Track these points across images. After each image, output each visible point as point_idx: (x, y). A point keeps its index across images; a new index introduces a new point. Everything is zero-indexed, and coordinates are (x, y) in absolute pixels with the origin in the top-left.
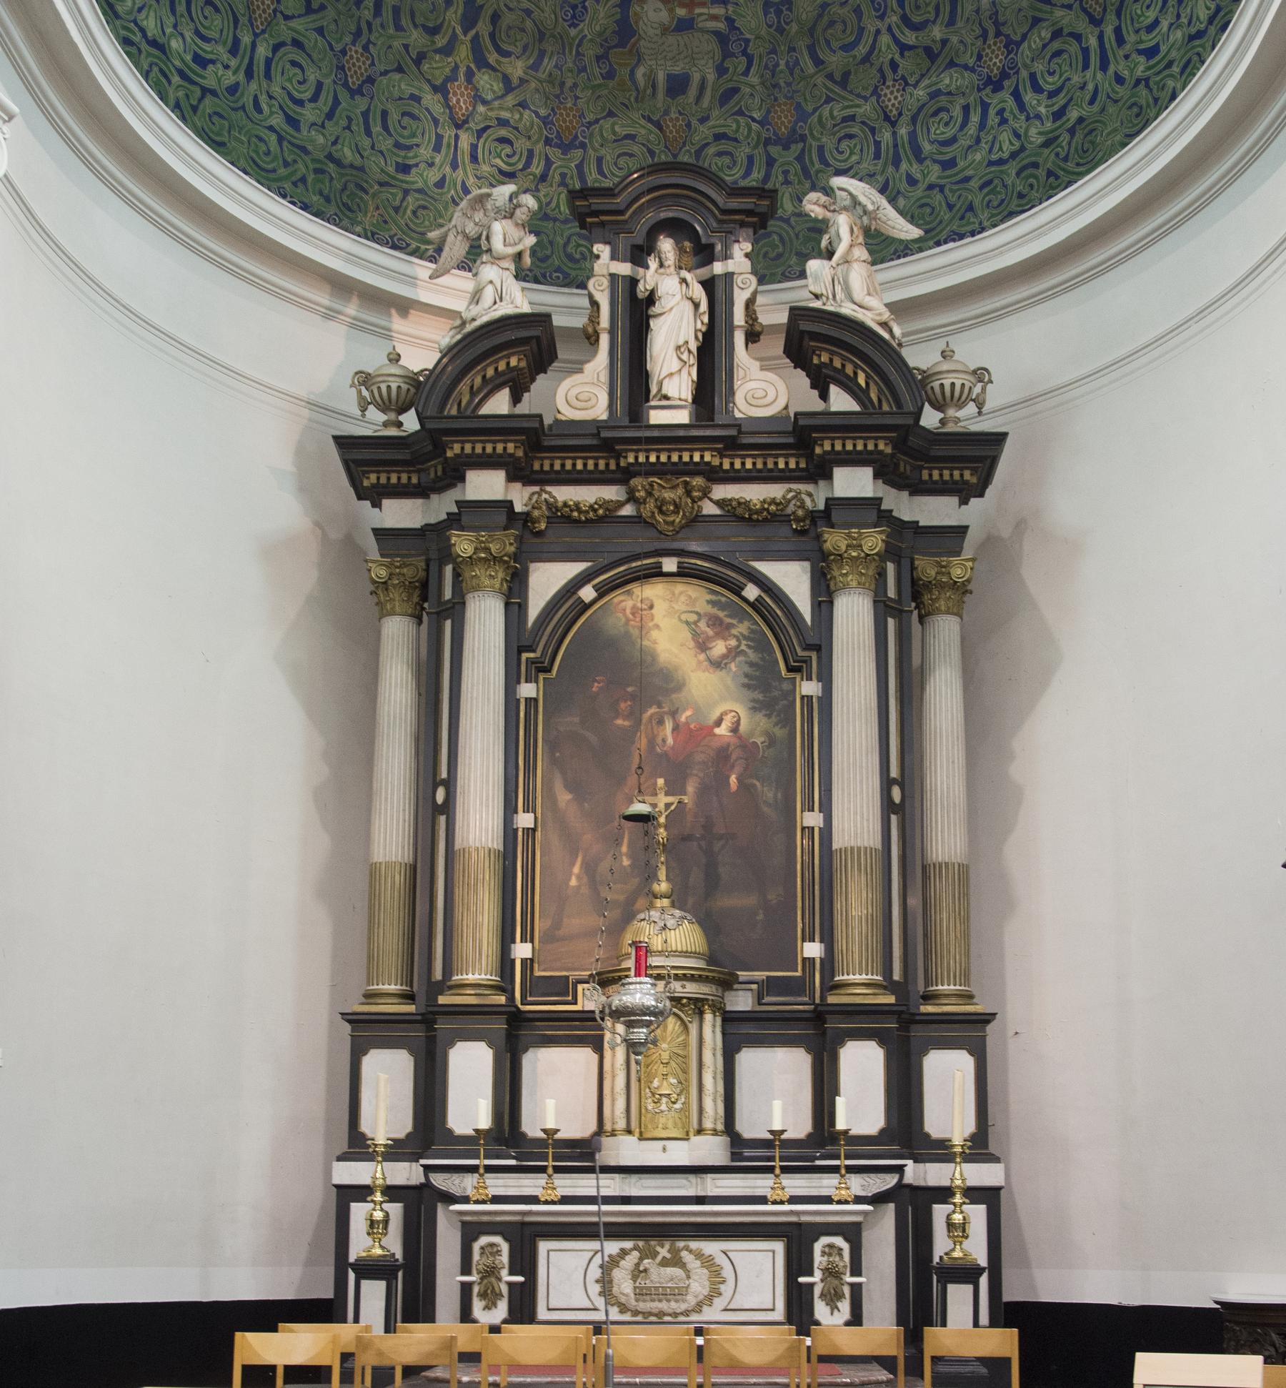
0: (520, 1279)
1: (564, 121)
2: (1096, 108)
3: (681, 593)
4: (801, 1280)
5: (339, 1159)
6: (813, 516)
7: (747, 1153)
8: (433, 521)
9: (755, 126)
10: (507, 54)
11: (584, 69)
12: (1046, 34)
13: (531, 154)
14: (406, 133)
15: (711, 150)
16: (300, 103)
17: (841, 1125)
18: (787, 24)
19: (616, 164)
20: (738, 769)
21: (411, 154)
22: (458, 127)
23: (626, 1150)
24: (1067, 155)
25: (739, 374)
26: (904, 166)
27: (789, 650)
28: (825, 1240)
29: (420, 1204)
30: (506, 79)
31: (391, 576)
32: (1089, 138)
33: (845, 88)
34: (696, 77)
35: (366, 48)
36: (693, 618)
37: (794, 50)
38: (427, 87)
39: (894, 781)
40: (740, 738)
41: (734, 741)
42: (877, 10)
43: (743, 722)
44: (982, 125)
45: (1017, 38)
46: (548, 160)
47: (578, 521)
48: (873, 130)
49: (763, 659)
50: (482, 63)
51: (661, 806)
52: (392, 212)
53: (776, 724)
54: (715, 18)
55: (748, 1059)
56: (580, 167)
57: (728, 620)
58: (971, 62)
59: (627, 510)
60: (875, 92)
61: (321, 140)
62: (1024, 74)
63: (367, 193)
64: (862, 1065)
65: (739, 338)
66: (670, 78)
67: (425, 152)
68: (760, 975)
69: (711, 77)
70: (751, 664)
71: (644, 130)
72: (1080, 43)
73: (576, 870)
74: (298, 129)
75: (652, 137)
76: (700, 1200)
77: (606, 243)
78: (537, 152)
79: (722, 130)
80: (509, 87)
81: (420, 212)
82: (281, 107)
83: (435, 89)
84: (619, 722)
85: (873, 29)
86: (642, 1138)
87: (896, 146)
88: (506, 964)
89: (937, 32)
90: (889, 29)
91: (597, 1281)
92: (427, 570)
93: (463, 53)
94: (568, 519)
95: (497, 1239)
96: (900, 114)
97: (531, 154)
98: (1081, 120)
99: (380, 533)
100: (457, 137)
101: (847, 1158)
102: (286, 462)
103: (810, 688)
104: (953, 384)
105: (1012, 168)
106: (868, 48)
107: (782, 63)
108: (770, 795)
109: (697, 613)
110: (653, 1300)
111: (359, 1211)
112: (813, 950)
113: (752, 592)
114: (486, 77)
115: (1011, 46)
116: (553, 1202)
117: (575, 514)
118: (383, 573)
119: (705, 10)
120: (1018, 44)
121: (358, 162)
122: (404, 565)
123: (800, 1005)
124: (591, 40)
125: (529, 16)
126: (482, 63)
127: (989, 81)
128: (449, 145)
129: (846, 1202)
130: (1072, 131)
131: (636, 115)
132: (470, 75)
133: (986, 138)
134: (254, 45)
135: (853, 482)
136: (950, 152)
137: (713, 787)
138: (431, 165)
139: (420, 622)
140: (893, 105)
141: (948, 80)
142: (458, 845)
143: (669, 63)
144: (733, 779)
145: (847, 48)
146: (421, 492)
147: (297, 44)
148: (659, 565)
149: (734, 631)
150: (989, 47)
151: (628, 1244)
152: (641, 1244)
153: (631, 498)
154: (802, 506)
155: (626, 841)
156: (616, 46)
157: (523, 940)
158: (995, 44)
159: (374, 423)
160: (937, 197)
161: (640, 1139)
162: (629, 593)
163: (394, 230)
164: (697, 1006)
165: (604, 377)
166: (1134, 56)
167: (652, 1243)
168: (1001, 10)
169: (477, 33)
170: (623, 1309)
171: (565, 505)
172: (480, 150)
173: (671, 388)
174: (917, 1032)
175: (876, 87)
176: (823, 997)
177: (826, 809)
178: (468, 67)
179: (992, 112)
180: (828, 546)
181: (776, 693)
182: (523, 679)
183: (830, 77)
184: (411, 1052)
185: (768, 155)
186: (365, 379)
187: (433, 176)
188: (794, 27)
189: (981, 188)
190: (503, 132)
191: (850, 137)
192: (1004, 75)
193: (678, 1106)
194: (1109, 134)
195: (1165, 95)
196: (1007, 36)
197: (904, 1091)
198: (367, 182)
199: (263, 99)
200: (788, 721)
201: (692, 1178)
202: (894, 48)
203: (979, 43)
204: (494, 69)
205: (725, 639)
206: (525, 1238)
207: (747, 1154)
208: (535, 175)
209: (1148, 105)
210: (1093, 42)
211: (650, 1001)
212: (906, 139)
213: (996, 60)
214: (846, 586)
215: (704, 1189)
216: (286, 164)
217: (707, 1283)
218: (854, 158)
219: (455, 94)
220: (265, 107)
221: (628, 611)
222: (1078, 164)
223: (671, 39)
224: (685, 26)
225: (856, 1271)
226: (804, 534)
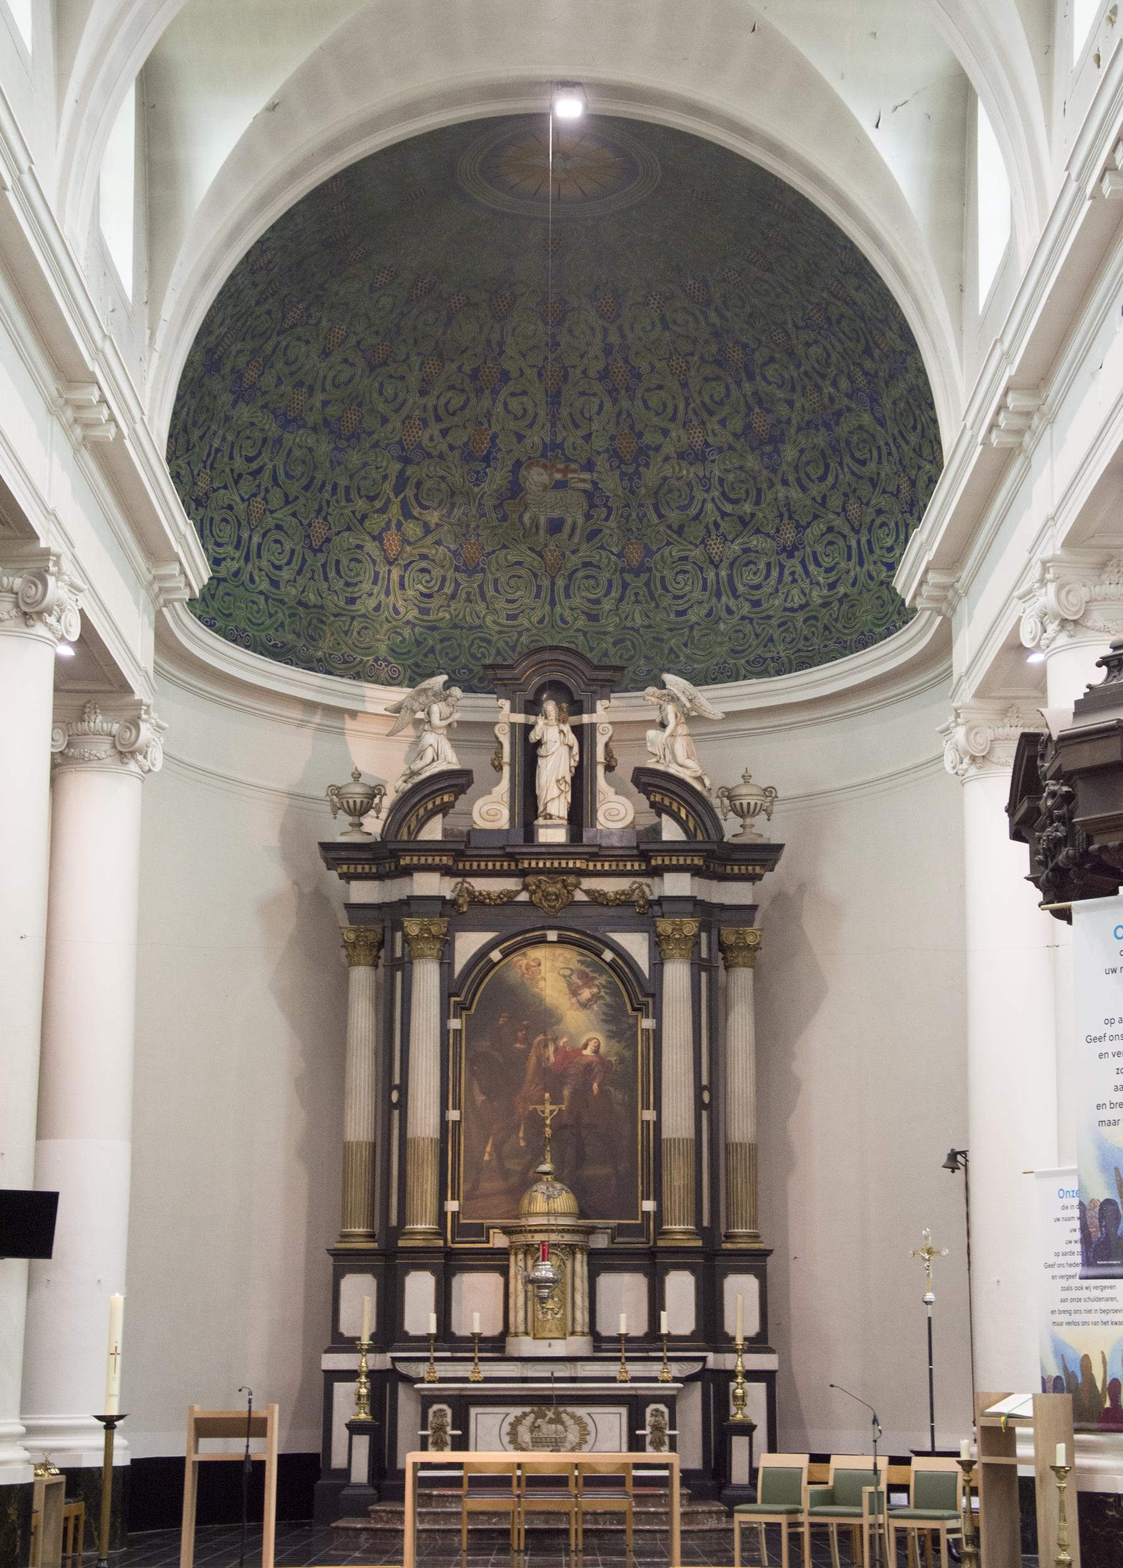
0: (459, 1432)
1: (469, 553)
2: (855, 590)
4: (638, 1432)
5: (326, 1352)
6: (651, 903)
7: (604, 1346)
8: (387, 900)
9: (613, 558)
11: (484, 515)
13: (444, 579)
14: (353, 574)
15: (580, 574)
16: (279, 568)
17: (664, 1330)
20: (598, 1079)
22: (390, 564)
23: (526, 1346)
25: (600, 797)
26: (724, 599)
27: (631, 996)
28: (653, 1406)
29: (383, 1386)
30: (426, 525)
33: (680, 536)
34: (569, 521)
35: (325, 519)
36: (568, 972)
37: (642, 505)
38: (367, 538)
39: (705, 1088)
40: (600, 1057)
41: (596, 1059)
44: (780, 581)
45: (804, 524)
46: (456, 582)
48: (701, 569)
50: (407, 514)
51: (547, 1111)
52: (343, 635)
54: (583, 481)
55: (605, 1281)
56: (481, 587)
57: (592, 974)
58: (772, 532)
59: (523, 897)
60: (703, 542)
61: (294, 592)
62: (808, 550)
64: (681, 1287)
65: (600, 770)
66: (551, 521)
67: (366, 586)
68: (613, 1222)
69: (580, 521)
70: (607, 1005)
71: (529, 558)
73: (488, 1149)
74: (278, 588)
75: (535, 564)
76: (573, 1380)
77: (507, 698)
78: (448, 577)
79: (588, 560)
80: (427, 529)
82: (267, 575)
83: (374, 538)
84: (518, 1045)
85: (701, 499)
86: (535, 1338)
87: (718, 583)
88: (442, 1214)
89: (748, 508)
90: (713, 500)
92: (383, 935)
93: (395, 510)
94: (483, 903)
95: (444, 1407)
96: (721, 561)
97: (444, 579)
98: (846, 595)
99: (349, 907)
100: (390, 571)
102: (272, 838)
103: (647, 1023)
104: (749, 804)
105: (800, 617)
107: (634, 515)
108: (620, 1096)
111: (343, 1391)
112: (649, 1206)
113: (608, 955)
114: (411, 525)
115: (800, 528)
116: (478, 1382)
120: (805, 528)
121: (319, 602)
122: (368, 930)
123: (638, 1243)
127: (784, 549)
128: (383, 578)
129: (667, 1382)
130: (841, 601)
131: (523, 547)
132: (399, 525)
133: (783, 590)
134: (250, 537)
135: (677, 885)
136: (757, 595)
137: (582, 1092)
138: (371, 595)
141: (755, 542)
142: (409, 1136)
144: (595, 1086)
145: (683, 508)
146: (379, 877)
147: (279, 527)
148: (545, 936)
149: (596, 982)
151: (527, 1409)
152: (536, 1409)
153: (525, 887)
154: (643, 896)
155: (522, 1128)
156: (509, 498)
157: (453, 1199)
159: (339, 830)
160: (748, 628)
162: (524, 954)
163: (345, 649)
164: (571, 1249)
165: (506, 798)
166: (879, 564)
168: (792, 503)
169: (405, 497)
171: (481, 894)
172: (406, 579)
173: (553, 809)
174: (720, 1262)
176: (655, 1242)
177: (658, 1107)
179: (786, 572)
180: (659, 929)
181: (625, 1026)
183: (669, 527)
184: (375, 1276)
185: (623, 580)
186: (337, 791)
187: (372, 603)
189: (780, 626)
190: (423, 564)
191: (685, 572)
192: (795, 548)
193: (558, 1316)
196: (797, 521)
197: (710, 1305)
199: (256, 573)
200: (632, 1044)
201: (568, 1364)
202: (717, 513)
203: (777, 521)
204: (418, 519)
205: (590, 988)
207: (604, 1345)
210: (854, 544)
211: (550, 1275)
212: (725, 579)
213: (789, 535)
214: (671, 957)
215: (576, 1372)
216: (271, 616)
218: (688, 588)
219: (389, 540)
220: (257, 579)
221: (524, 968)
222: (844, 627)
224: (561, 485)
225: (673, 1426)
226: (644, 913)
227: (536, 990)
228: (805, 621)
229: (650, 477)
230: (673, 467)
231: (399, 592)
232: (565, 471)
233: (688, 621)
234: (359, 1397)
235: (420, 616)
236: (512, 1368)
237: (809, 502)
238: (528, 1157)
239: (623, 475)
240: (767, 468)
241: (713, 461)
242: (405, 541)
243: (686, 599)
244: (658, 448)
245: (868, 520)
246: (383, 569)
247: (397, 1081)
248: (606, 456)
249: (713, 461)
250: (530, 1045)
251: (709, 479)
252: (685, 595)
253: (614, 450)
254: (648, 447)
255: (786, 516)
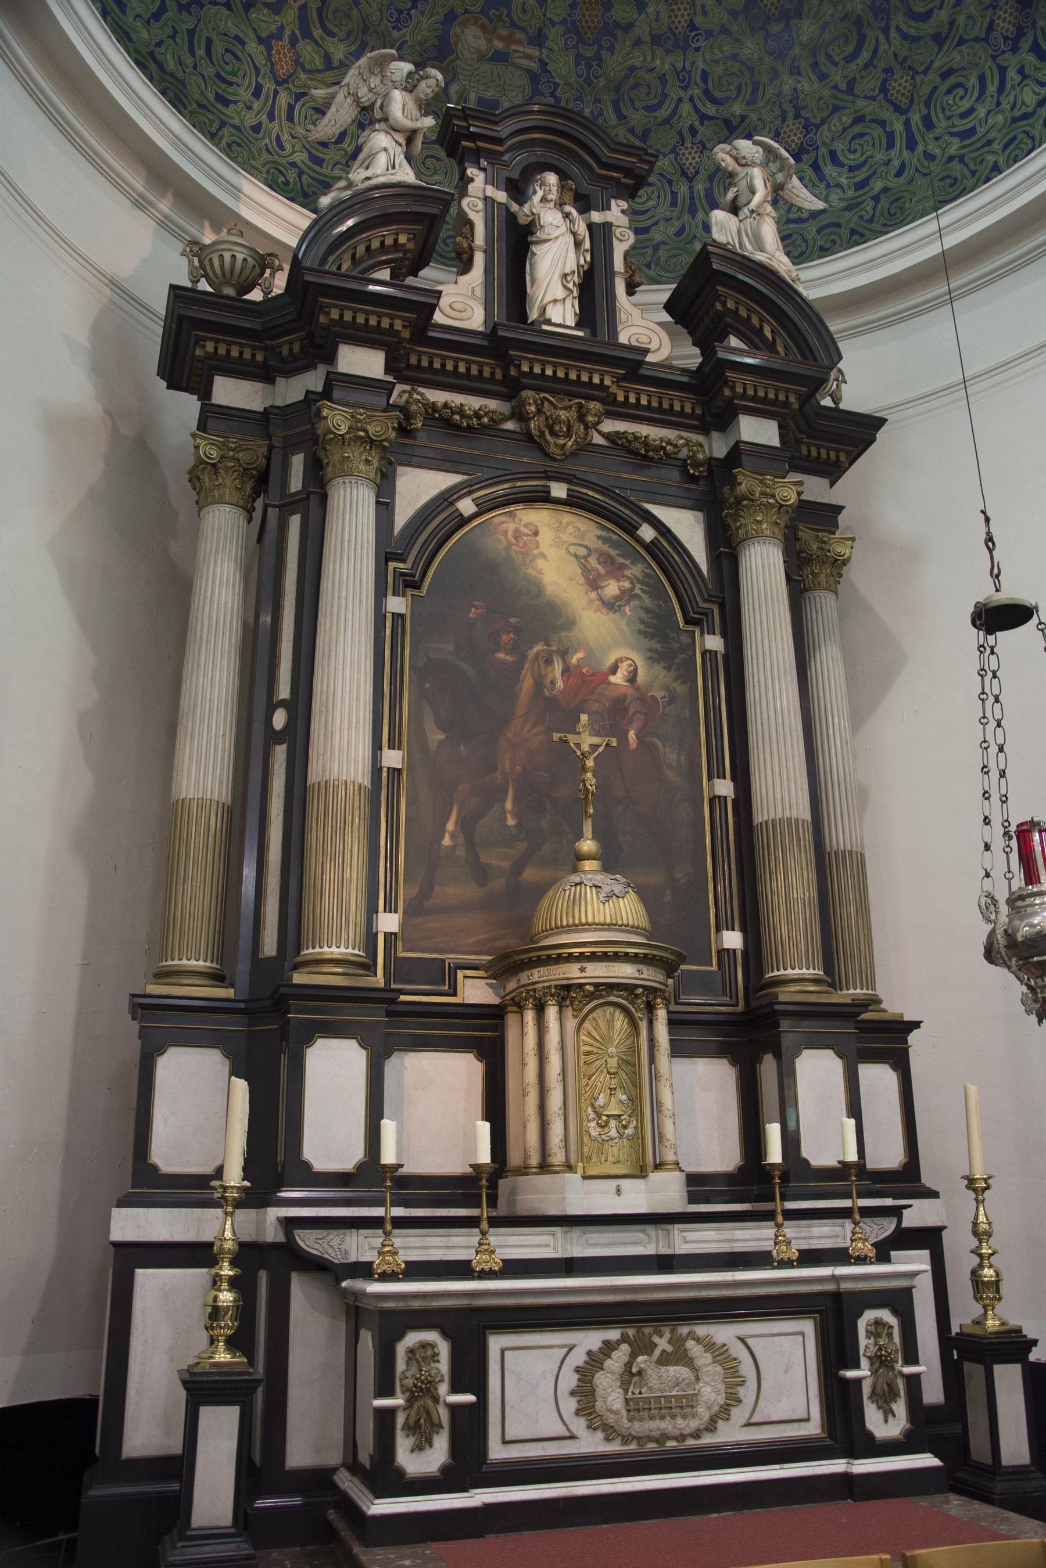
3: (568, 524)
5: (120, 1204)
10: (332, 35)
12: (847, 120)
14: (228, 68)
18: (596, 78)
19: (423, 163)
20: (637, 724)
21: (230, 90)
24: (873, 217)
25: (622, 317)
28: (870, 1315)
30: (327, 57)
31: (222, 458)
32: (896, 204)
36: (582, 552)
37: (599, 101)
38: (252, 35)
40: (638, 689)
42: (682, 82)
43: (640, 672)
47: (457, 427)
48: (670, 182)
49: (659, 606)
50: (307, 34)
53: (676, 679)
59: (510, 425)
60: (673, 150)
61: (146, 35)
62: (823, 150)
63: (185, 108)
70: (647, 610)
72: (884, 128)
73: (450, 826)
76: (665, 1263)
81: (234, 147)
83: (260, 40)
84: (501, 655)
87: (692, 198)
89: (737, 109)
90: (691, 99)
91: (573, 1393)
92: (268, 458)
95: (432, 1336)
96: (697, 172)
98: (885, 190)
100: (276, 92)
101: (859, 1196)
102: (82, 335)
106: (669, 112)
108: (674, 757)
109: (586, 547)
110: (652, 1418)
111: (150, 1283)
113: (647, 533)
114: (309, 48)
117: (457, 417)
118: (214, 454)
119: (521, 49)
122: (238, 449)
124: (411, 47)
125: (357, 6)
126: (307, 34)
128: (267, 96)
130: (876, 199)
139: (250, 520)
140: (691, 164)
142: (314, 775)
143: (481, 88)
144: (632, 734)
146: (265, 374)
149: (628, 573)
150: (788, 126)
152: (631, 1332)
158: (794, 124)
161: (585, 1177)
165: (480, 292)
166: (946, 137)
167: (647, 1330)
168: (802, 96)
170: (610, 1432)
172: (296, 112)
175: (675, 147)
178: (293, 32)
182: (390, 591)
183: (631, 131)
184: (227, 1054)
188: (602, 82)
193: (629, 1131)
194: (918, 201)
195: (984, 170)
196: (806, 119)
198: (186, 97)
200: (686, 673)
201: (651, 1229)
206: (469, 1332)
208: (346, 152)
209: (964, 177)
210: (898, 127)
212: (702, 194)
214: (759, 535)
217: (722, 1387)
218: (651, 203)
221: (510, 534)
222: (884, 225)
223: (486, 67)
224: (500, 57)
227: (530, 571)
228: (819, 231)
229: (615, 64)
230: (645, 56)
231: (285, 124)
232: (508, 40)
233: (651, 240)
234: (215, 1313)
235: (310, 164)
236: (547, 1239)
237: (826, 92)
238: (522, 846)
239: (578, 57)
240: (770, 54)
241: (697, 49)
242: (298, 63)
243: (648, 215)
244: (628, 27)
245: (925, 90)
246: (269, 86)
247: (284, 692)
248: (560, 28)
249: (697, 49)
250: (523, 658)
251: (689, 73)
252: (649, 210)
253: (573, 23)
254: (617, 24)
255: (791, 114)
